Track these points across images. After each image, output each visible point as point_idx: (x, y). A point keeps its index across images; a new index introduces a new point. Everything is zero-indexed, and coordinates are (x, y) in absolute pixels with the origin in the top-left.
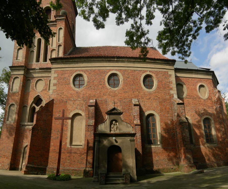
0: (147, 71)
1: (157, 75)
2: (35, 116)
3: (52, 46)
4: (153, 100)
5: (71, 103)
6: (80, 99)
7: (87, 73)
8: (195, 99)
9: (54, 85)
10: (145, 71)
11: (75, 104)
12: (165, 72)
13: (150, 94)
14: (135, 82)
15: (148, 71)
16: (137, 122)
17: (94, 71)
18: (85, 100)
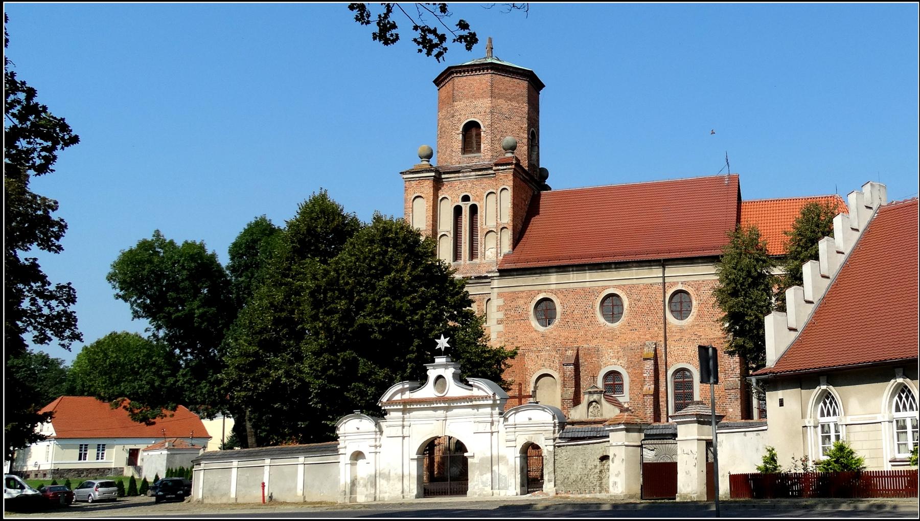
3: (473, 255)
5: (533, 355)
7: (559, 295)
9: (500, 322)
13: (682, 330)
17: (573, 290)
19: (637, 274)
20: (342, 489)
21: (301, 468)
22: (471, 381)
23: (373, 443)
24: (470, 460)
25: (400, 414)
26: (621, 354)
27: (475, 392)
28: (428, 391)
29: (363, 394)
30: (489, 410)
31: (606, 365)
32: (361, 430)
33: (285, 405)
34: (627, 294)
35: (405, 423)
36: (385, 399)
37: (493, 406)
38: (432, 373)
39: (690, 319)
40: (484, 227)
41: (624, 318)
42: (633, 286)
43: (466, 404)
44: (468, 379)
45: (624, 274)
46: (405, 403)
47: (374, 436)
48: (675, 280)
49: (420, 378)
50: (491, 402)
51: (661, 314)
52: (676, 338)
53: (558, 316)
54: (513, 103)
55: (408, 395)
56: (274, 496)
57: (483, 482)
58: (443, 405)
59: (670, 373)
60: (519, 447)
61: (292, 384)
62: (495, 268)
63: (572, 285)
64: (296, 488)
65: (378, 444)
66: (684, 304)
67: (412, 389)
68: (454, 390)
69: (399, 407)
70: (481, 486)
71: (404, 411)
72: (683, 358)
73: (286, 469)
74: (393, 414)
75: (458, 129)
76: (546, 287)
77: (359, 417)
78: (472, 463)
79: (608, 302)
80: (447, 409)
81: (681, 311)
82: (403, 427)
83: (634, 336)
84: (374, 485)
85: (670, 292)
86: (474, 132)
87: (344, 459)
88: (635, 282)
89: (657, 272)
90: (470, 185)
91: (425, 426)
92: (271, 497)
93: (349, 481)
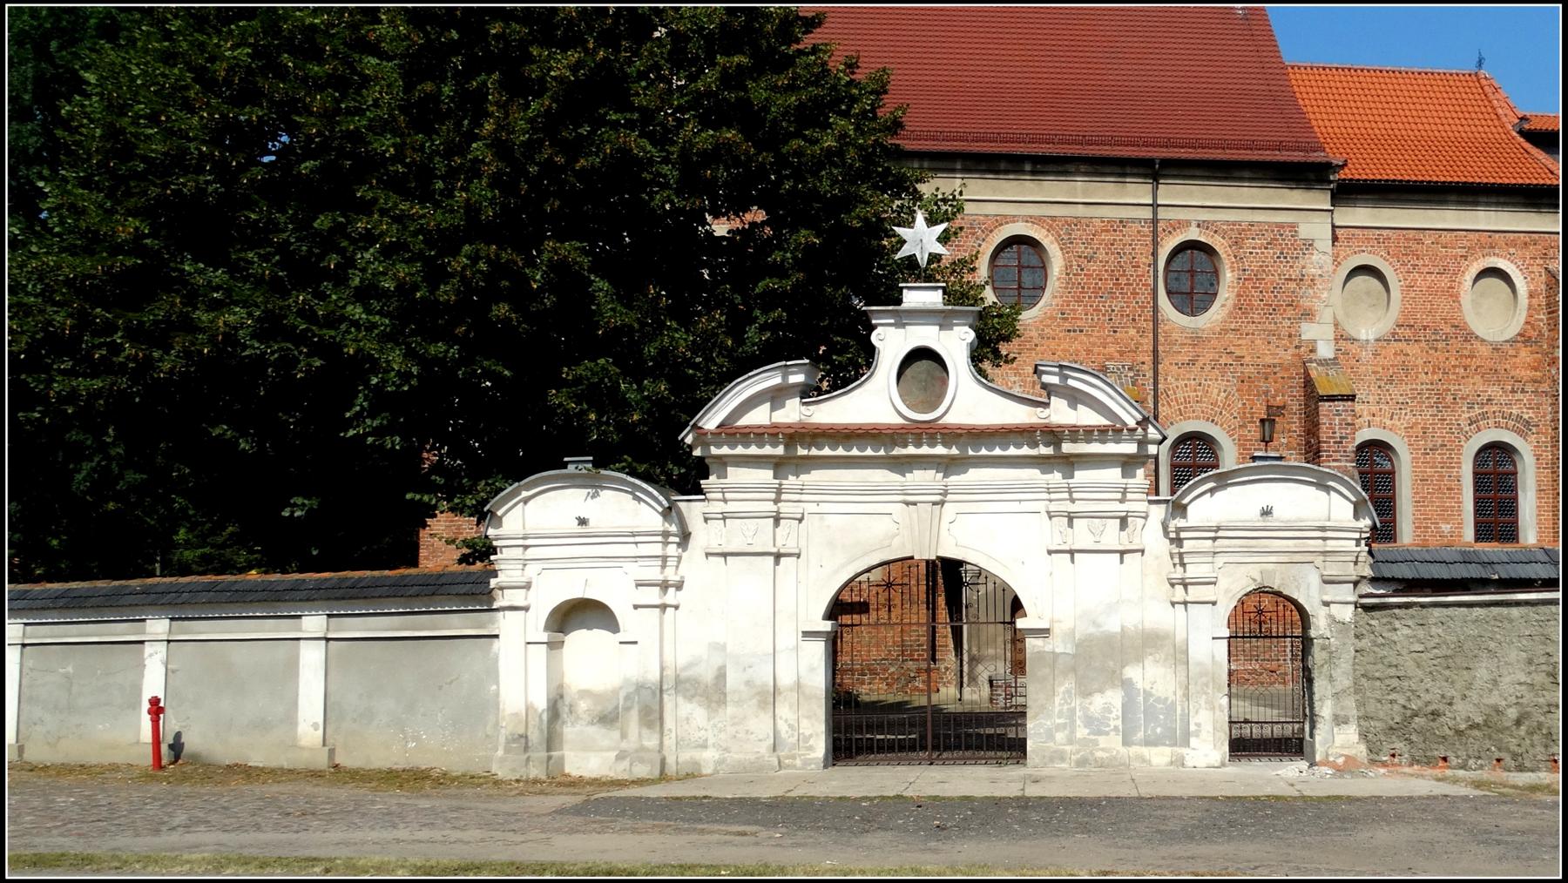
0: (1188, 223)
4: (1208, 368)
8: (1440, 345)
10: (1003, 220)
12: (1280, 226)
13: (1196, 340)
14: (1123, 281)
15: (1194, 224)
19: (1085, 194)
20: (508, 728)
21: (312, 658)
23: (653, 573)
24: (1032, 644)
25: (765, 475)
28: (873, 401)
29: (603, 397)
30: (1113, 474)
32: (594, 525)
33: (244, 435)
34: (1059, 239)
35: (785, 508)
36: (711, 420)
37: (1128, 464)
38: (891, 342)
39: (1216, 314)
42: (1077, 221)
43: (1026, 451)
45: (1052, 189)
46: (797, 435)
47: (657, 549)
49: (845, 363)
50: (1130, 448)
51: (1144, 296)
55: (793, 412)
56: (191, 742)
57: (1089, 721)
58: (940, 450)
60: (1226, 606)
61: (287, 362)
64: (291, 718)
65: (671, 575)
66: (1199, 277)
67: (808, 392)
69: (768, 450)
70: (1082, 732)
71: (780, 466)
72: (1197, 407)
73: (239, 653)
74: (736, 475)
77: (593, 484)
78: (1041, 655)
79: (1009, 258)
80: (948, 466)
81: (1190, 294)
82: (777, 520)
83: (1076, 345)
84: (653, 717)
85: (1168, 245)
87: (516, 633)
88: (1081, 211)
89: (1137, 192)
91: (859, 524)
92: (177, 747)
93: (541, 703)
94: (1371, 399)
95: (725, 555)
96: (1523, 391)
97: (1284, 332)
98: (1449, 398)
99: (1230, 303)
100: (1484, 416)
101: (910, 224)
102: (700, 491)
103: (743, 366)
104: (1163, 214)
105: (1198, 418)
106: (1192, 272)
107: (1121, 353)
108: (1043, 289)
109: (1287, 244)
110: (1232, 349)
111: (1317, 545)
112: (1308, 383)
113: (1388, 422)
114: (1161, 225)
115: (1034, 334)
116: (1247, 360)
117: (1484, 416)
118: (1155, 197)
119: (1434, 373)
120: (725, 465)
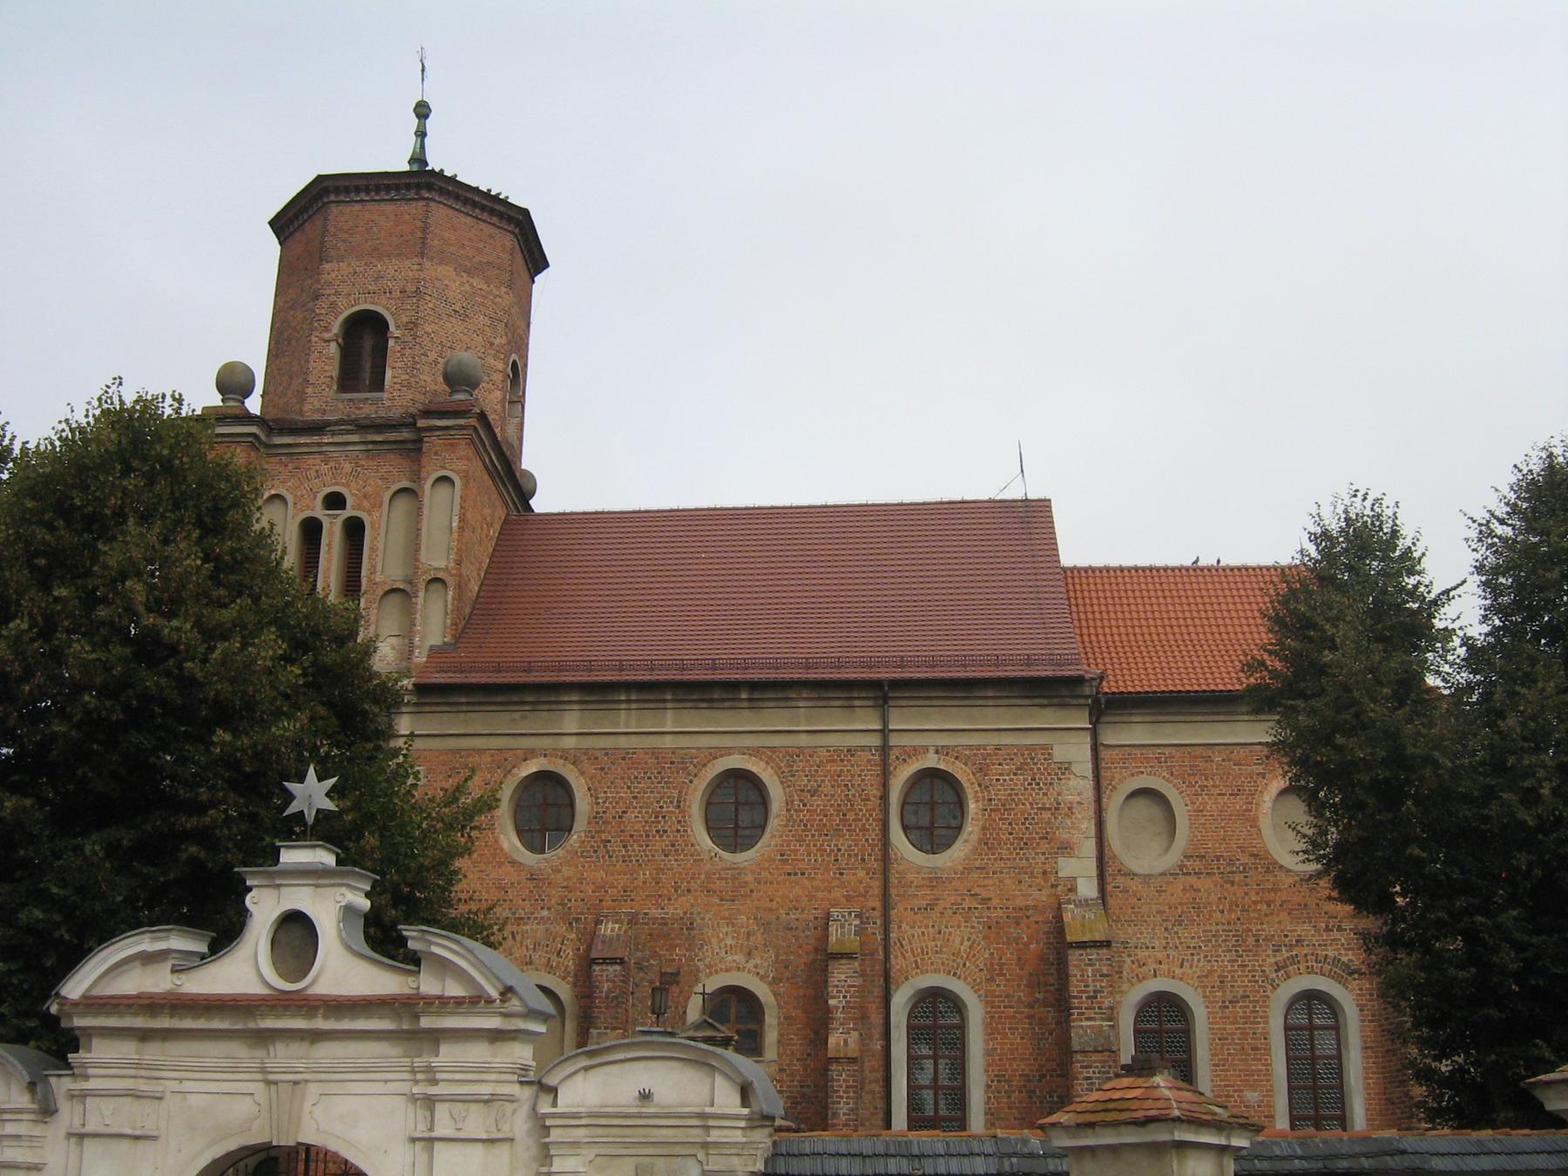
0: (926, 749)
1: (982, 770)
2: (278, 440)
6: (545, 913)
8: (1237, 878)
10: (917, 751)
11: (518, 938)
12: (1030, 748)
13: (935, 880)
14: (850, 816)
15: (932, 750)
16: (846, 1041)
17: (626, 755)
18: (577, 920)
22: (415, 937)
26: (759, 938)
27: (428, 984)
28: (246, 969)
31: (712, 970)
34: (779, 772)
36: (76, 987)
38: (264, 907)
39: (958, 852)
40: (378, 578)
41: (767, 843)
42: (801, 750)
44: (409, 931)
45: (774, 719)
48: (918, 740)
49: (224, 931)
51: (874, 834)
52: (916, 903)
53: (580, 824)
54: (475, 281)
55: (159, 981)
59: (901, 1000)
62: (99, 1052)
63: (622, 742)
68: (342, 969)
75: (327, 329)
76: (546, 742)
81: (930, 829)
83: (797, 890)
85: (902, 775)
86: (368, 343)
88: (803, 740)
90: (347, 467)
94: (1157, 943)
95: (137, 1138)
96: (1340, 929)
97: (1038, 870)
98: (1251, 940)
99: (974, 837)
100: (1293, 960)
101: (301, 778)
102: (69, 1066)
103: (105, 933)
104: (894, 740)
105: (937, 971)
106: (935, 806)
107: (848, 898)
108: (763, 827)
109: (1039, 767)
110: (978, 890)
111: (696, 1135)
112: (1059, 927)
113: (1178, 971)
114: (893, 754)
115: (749, 878)
116: (995, 901)
117: (1293, 960)
118: (885, 722)
119: (1231, 910)
120: (90, 1037)
